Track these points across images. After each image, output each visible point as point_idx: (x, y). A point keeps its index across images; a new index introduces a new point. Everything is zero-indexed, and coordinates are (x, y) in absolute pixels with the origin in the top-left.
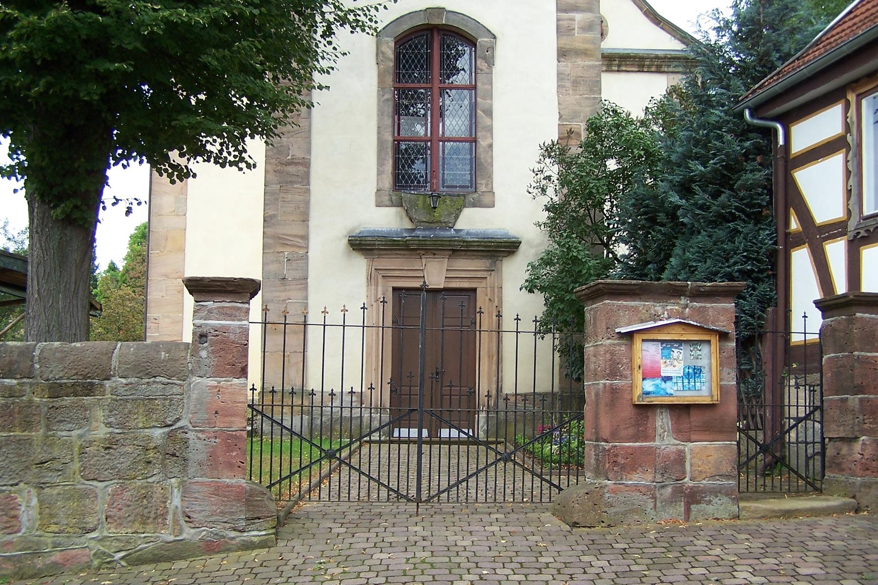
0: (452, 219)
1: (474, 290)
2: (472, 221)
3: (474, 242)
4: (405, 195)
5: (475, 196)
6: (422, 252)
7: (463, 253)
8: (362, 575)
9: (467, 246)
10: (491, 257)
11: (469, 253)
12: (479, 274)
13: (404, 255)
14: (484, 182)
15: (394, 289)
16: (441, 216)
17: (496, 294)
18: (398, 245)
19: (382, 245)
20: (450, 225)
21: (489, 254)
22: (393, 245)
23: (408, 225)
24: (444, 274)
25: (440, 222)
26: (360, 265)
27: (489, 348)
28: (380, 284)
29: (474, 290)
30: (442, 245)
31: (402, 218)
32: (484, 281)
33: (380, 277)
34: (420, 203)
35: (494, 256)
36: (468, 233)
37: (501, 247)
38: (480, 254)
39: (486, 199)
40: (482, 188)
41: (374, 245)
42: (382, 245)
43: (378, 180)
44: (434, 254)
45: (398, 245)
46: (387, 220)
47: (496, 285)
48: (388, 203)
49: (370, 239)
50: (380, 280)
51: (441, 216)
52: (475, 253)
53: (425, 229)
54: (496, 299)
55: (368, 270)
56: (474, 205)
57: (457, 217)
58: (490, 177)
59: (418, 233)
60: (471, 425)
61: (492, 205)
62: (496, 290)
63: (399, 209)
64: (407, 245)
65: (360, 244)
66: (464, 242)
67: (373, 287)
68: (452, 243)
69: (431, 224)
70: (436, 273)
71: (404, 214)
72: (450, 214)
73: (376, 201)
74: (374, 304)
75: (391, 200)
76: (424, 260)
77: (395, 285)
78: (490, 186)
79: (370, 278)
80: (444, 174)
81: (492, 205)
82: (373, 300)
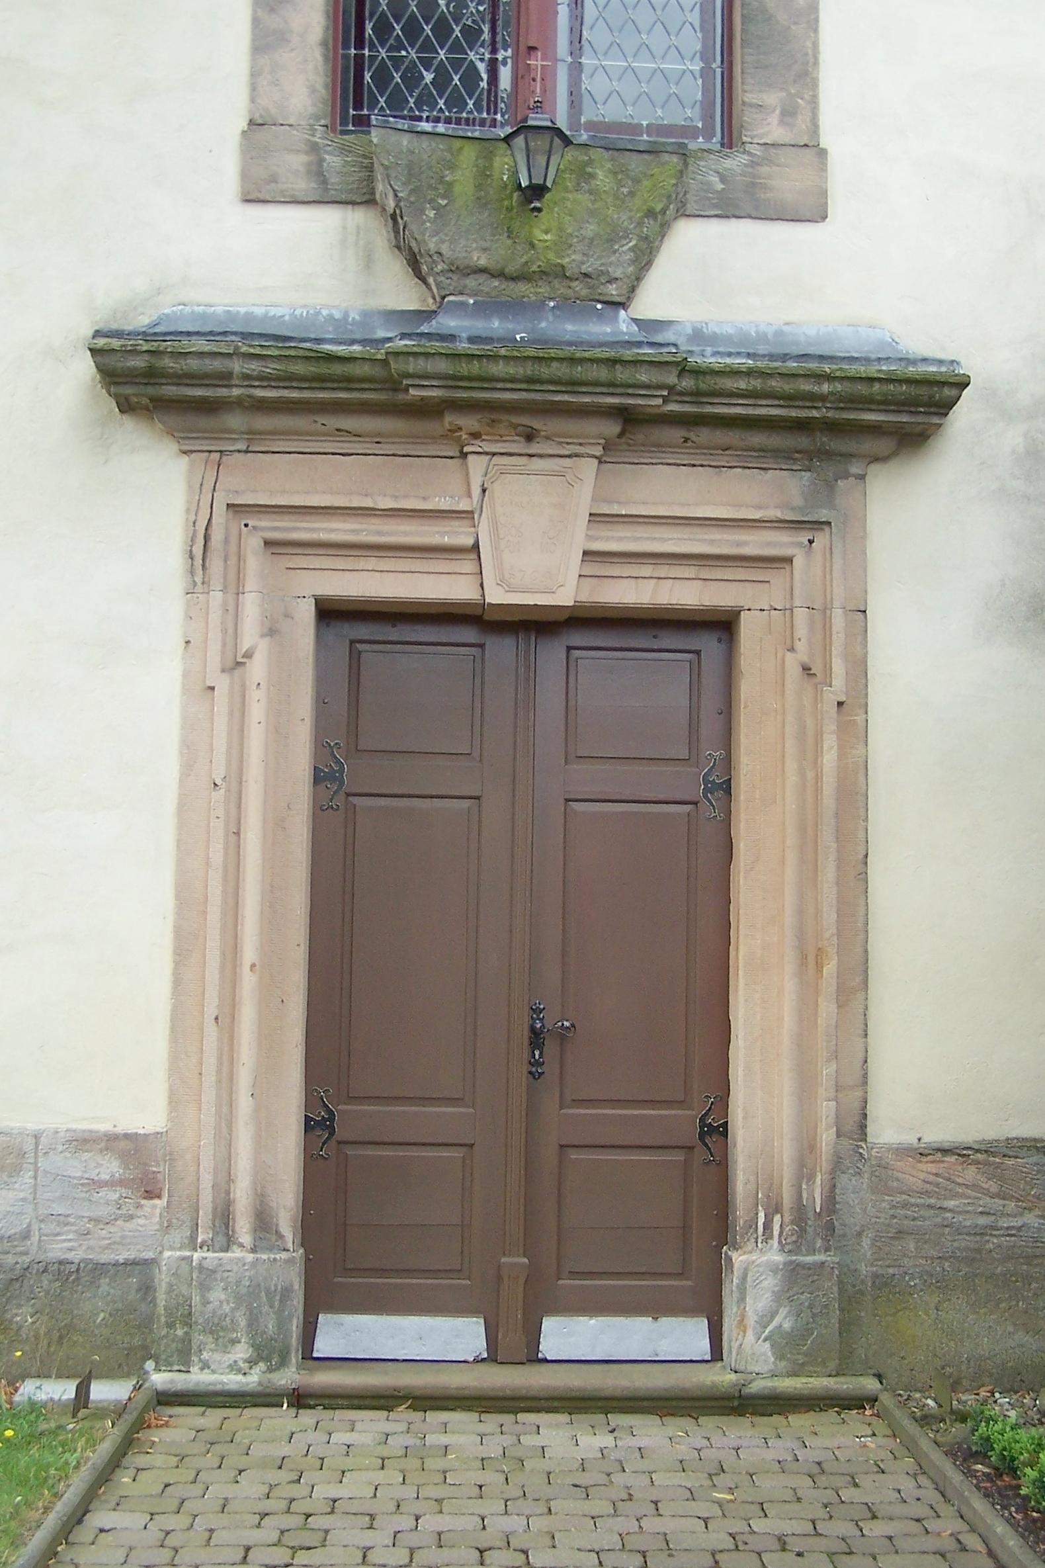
0: (620, 264)
1: (723, 625)
2: (718, 287)
3: (734, 373)
4: (388, 139)
5: (734, 163)
6: (469, 422)
7: (675, 434)
8: (283, 1505)
9: (697, 395)
10: (811, 458)
11: (703, 435)
12: (754, 543)
13: (378, 438)
14: (772, 98)
15: (330, 613)
16: (563, 244)
17: (837, 648)
18: (348, 382)
19: (265, 380)
20: (613, 291)
21: (803, 441)
22: (320, 381)
23: (403, 295)
24: (579, 537)
25: (561, 273)
26: (157, 482)
27: (800, 912)
28: (251, 582)
29: (723, 625)
30: (573, 385)
31: (368, 261)
32: (777, 578)
33: (253, 543)
34: (463, 178)
35: (826, 455)
36: (698, 336)
37: (867, 403)
38: (758, 439)
39: (786, 181)
40: (764, 127)
41: (224, 378)
42: (265, 380)
43: (255, 74)
44: (530, 437)
45: (348, 382)
46: (305, 268)
47: (838, 593)
48: (302, 185)
49: (201, 345)
50: (254, 561)
51: (563, 244)
52: (733, 437)
53: (484, 308)
54: (838, 668)
55: (193, 508)
56: (727, 208)
57: (644, 258)
58: (804, 74)
59: (449, 323)
60: (710, 1306)
61: (814, 211)
62: (838, 620)
63: (357, 217)
64: (394, 384)
65: (151, 375)
66: (683, 368)
67: (216, 597)
68: (621, 374)
69: (515, 281)
70: (534, 531)
71: (381, 238)
72: (612, 238)
73: (245, 175)
74: (223, 684)
75: (318, 172)
76: (476, 465)
77: (320, 592)
78: (802, 121)
79: (201, 552)
80: (576, 69)
81: (814, 211)
82: (214, 660)
